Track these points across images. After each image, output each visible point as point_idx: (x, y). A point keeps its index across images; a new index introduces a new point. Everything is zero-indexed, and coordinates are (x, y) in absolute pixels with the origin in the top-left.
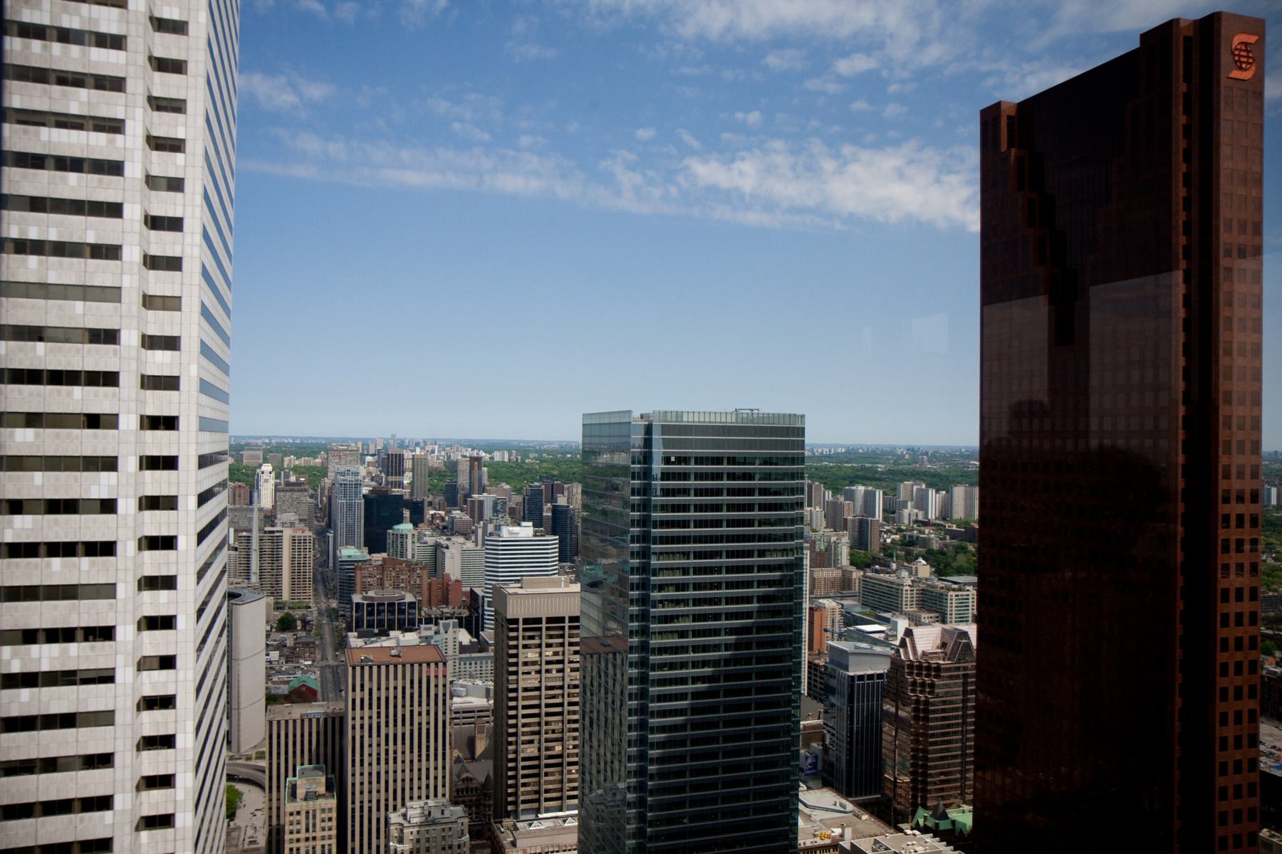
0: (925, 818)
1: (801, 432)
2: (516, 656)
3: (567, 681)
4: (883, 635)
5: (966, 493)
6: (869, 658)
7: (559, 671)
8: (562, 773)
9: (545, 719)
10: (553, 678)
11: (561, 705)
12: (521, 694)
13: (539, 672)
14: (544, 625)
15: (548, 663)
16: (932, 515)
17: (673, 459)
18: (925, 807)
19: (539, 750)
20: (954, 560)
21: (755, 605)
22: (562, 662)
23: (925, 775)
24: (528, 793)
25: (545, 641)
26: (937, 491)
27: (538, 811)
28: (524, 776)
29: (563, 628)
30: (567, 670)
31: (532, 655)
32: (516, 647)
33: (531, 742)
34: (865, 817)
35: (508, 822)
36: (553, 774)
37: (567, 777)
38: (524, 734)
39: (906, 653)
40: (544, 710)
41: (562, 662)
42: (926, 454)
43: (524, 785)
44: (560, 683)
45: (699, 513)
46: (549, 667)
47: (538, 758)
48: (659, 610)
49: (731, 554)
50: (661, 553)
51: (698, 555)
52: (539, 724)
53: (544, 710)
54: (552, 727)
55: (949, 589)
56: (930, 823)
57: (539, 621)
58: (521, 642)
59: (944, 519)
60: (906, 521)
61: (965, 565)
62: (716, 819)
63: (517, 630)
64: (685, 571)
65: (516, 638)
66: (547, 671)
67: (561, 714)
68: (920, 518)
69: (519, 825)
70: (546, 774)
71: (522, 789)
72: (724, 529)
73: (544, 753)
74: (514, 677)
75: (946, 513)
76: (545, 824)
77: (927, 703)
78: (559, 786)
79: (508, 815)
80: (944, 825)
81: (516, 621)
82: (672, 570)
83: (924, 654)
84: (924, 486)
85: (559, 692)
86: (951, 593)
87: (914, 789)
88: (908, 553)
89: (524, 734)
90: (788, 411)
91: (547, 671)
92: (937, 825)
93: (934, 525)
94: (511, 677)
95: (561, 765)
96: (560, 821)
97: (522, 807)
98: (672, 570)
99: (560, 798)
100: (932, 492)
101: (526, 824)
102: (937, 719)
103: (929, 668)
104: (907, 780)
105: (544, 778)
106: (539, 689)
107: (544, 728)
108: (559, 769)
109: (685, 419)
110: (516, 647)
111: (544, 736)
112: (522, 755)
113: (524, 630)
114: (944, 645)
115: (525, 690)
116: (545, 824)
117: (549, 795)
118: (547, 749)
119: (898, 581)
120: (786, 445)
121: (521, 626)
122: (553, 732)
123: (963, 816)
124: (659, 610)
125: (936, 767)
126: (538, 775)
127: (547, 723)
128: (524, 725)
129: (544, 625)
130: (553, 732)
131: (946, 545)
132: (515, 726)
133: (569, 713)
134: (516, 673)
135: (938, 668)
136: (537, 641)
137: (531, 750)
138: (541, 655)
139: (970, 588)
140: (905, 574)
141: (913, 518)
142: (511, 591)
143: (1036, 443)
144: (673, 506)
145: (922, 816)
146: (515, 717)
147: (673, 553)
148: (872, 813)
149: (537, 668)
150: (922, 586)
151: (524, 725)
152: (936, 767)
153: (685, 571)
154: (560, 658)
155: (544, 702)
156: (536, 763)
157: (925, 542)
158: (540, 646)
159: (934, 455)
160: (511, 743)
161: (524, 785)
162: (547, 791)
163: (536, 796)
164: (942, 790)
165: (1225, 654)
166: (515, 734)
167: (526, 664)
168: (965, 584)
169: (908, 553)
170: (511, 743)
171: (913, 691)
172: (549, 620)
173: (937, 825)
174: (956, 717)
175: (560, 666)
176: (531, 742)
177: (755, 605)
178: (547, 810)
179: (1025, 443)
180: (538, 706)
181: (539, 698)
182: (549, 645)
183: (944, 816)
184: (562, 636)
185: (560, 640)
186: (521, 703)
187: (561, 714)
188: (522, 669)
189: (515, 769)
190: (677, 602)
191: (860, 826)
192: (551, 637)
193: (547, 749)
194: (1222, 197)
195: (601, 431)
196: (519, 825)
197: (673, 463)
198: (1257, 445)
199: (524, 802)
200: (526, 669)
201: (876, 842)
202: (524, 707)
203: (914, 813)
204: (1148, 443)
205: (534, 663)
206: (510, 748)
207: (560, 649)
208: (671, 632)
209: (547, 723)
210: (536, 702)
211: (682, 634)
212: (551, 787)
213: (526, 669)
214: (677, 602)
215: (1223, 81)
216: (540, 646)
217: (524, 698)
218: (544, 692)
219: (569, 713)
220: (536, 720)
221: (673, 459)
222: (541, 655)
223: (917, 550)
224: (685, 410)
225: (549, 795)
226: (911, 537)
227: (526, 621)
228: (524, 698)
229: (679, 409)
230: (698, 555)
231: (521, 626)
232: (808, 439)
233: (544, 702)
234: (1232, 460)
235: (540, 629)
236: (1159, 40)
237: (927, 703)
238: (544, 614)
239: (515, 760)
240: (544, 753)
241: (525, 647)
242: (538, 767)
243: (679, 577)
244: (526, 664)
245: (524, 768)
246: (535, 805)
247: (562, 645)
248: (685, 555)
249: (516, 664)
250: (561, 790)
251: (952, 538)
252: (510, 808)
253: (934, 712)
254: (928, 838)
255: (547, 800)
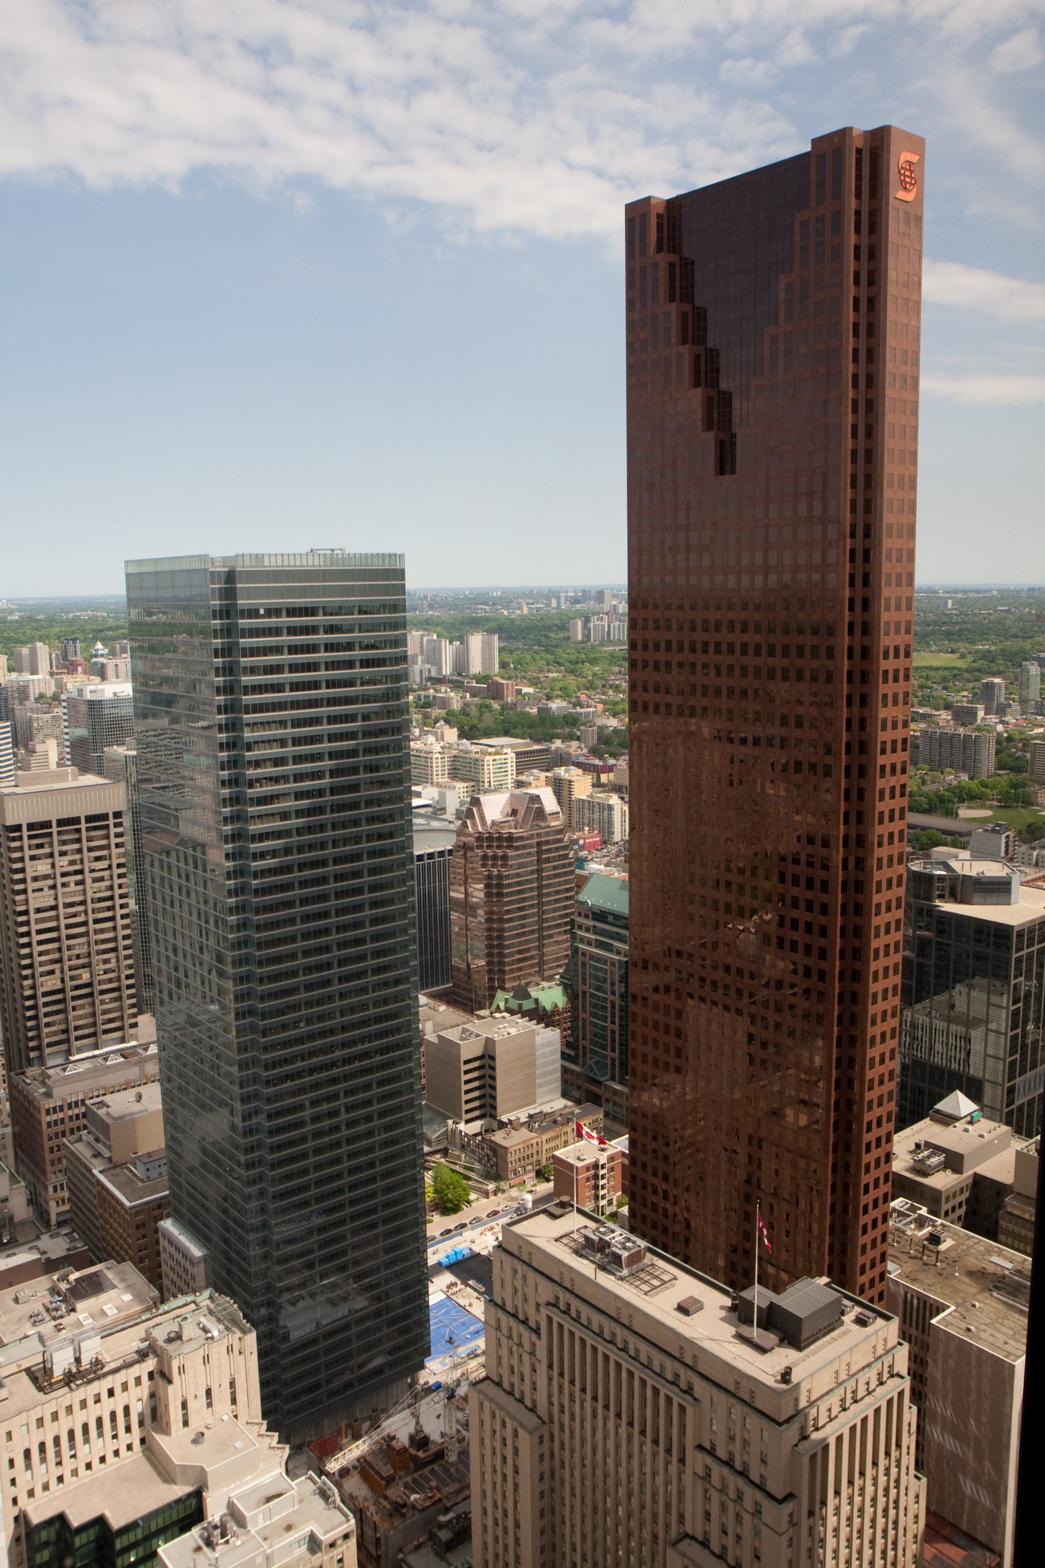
0: (506, 1001)
1: (400, 574)
2: (23, 870)
3: (90, 895)
4: (430, 809)
5: (483, 642)
6: (427, 834)
7: (77, 883)
8: (93, 1004)
9: (66, 943)
10: (71, 892)
11: (85, 923)
12: (33, 916)
13: (53, 887)
14: (55, 830)
15: (63, 875)
16: (447, 670)
17: (262, 612)
18: (503, 989)
19: (63, 980)
20: (480, 720)
21: (327, 781)
22: (81, 872)
23: (501, 955)
24: (54, 1033)
25: (57, 849)
26: (451, 642)
27: (69, 1052)
28: (46, 1015)
29: (79, 831)
30: (89, 881)
31: (42, 867)
32: (21, 860)
33: (52, 972)
34: (443, 1008)
35: (33, 1071)
36: (82, 1007)
37: (100, 1008)
38: (41, 964)
39: (474, 825)
40: (64, 932)
41: (81, 872)
42: (425, 597)
43: (48, 1025)
44: (81, 898)
45: (290, 675)
46: (66, 879)
47: (62, 991)
48: (257, 791)
49: (332, 719)
50: (255, 724)
51: (297, 723)
52: (60, 950)
53: (64, 932)
54: (76, 952)
55: (486, 753)
56: (514, 1004)
57: (47, 824)
58: (28, 853)
59: (460, 674)
60: (418, 680)
61: (493, 726)
62: (368, 1009)
63: (20, 838)
64: (283, 743)
65: (21, 849)
66: (64, 885)
67: (86, 934)
68: (434, 674)
69: (50, 1072)
70: (74, 1009)
71: (46, 1030)
72: (287, 695)
73: (69, 984)
74: (22, 897)
75: (461, 664)
76: (82, 1068)
77: (500, 877)
78: (91, 1020)
79: (30, 1062)
80: (528, 1005)
81: (18, 828)
82: (268, 742)
83: (493, 823)
84: (435, 637)
85: (81, 908)
86: (488, 758)
87: (490, 972)
88: (426, 716)
89: (41, 964)
90: (387, 551)
91: (64, 885)
92: (520, 1005)
93: (451, 681)
94: (18, 898)
95: (91, 995)
96: (100, 1060)
97: (48, 1051)
98: (268, 742)
99: (121, 1028)
100: (445, 644)
101: (58, 1069)
102: (511, 894)
103: (500, 839)
104: (482, 963)
105: (72, 1014)
106: (55, 908)
107: (66, 954)
108: (89, 1000)
109: (267, 563)
110: (21, 860)
111: (67, 964)
112: (42, 990)
113: (30, 837)
114: (514, 812)
115: (38, 910)
116: (82, 1068)
117: (80, 1033)
118: (72, 978)
119: (426, 748)
120: (385, 590)
121: (25, 833)
122: (78, 957)
123: (551, 995)
124: (257, 791)
125: (512, 946)
126: (63, 1011)
127: (69, 948)
128: (41, 954)
129: (55, 830)
130: (78, 957)
131: (467, 704)
132: (30, 956)
133: (96, 932)
134: (24, 891)
135: (510, 838)
136: (47, 850)
137: (52, 983)
138: (53, 866)
139: (508, 751)
140: (431, 739)
141: (426, 675)
142: (6, 791)
143: (693, 579)
144: (265, 667)
145: (501, 998)
146: (29, 945)
147: (268, 723)
148: (448, 1003)
149: (50, 882)
150: (455, 752)
151: (41, 954)
152: (512, 946)
153: (283, 743)
154: (78, 867)
155: (63, 922)
156: (59, 996)
157: (444, 703)
158: (51, 855)
159: (433, 599)
160: (26, 978)
161: (48, 1025)
162: (76, 1028)
163: (64, 1036)
164: (520, 969)
165: (894, 778)
166: (30, 966)
167: (35, 879)
168: (502, 747)
169: (426, 716)
170: (26, 978)
171: (484, 865)
172: (61, 823)
173: (520, 1005)
174: (531, 889)
175: (79, 877)
176: (52, 972)
177: (327, 781)
178: (80, 1050)
179: (745, 580)
180: (57, 929)
181: (57, 918)
182: (63, 854)
183: (528, 996)
184: (79, 840)
185: (76, 846)
186: (34, 927)
187: (86, 934)
188: (31, 886)
189: (35, 1007)
190: (275, 780)
191: (439, 1018)
192: (64, 843)
193: (72, 978)
194: (889, 324)
195: (141, 580)
196: (50, 1072)
197: (263, 617)
198: (911, 576)
199: (50, 1045)
200: (37, 885)
201: (464, 1031)
202: (39, 932)
203: (492, 997)
204: (816, 577)
205: (46, 877)
206: (26, 983)
207: (77, 857)
208: (273, 815)
209: (69, 948)
210: (53, 924)
211: (284, 815)
212: (81, 1022)
213: (37, 885)
214: (275, 780)
215: (891, 200)
216: (51, 855)
217: (38, 921)
218: (62, 911)
219: (96, 932)
220: (55, 945)
221: (262, 612)
222: (53, 866)
223: (436, 712)
224: (266, 551)
225: (80, 1033)
226: (426, 697)
227: (31, 826)
228: (38, 921)
229: (260, 551)
230: (297, 723)
231: (25, 833)
232: (412, 583)
233: (63, 922)
234: (887, 592)
235: (50, 834)
236: (830, 148)
237: (500, 877)
238: (81, 810)
239: (34, 997)
240: (69, 984)
241: (33, 858)
242: (63, 1001)
243: (276, 751)
244: (35, 879)
245: (45, 1005)
246: (64, 1047)
247: (79, 851)
248: (282, 723)
249: (23, 881)
250: (94, 1024)
251: (473, 696)
252: (32, 1055)
253: (509, 886)
254: (517, 1018)
255: (77, 1039)
